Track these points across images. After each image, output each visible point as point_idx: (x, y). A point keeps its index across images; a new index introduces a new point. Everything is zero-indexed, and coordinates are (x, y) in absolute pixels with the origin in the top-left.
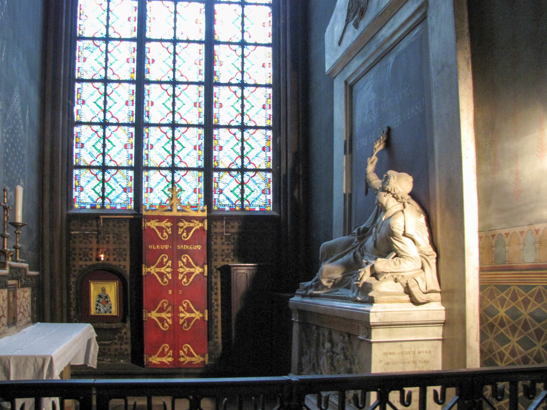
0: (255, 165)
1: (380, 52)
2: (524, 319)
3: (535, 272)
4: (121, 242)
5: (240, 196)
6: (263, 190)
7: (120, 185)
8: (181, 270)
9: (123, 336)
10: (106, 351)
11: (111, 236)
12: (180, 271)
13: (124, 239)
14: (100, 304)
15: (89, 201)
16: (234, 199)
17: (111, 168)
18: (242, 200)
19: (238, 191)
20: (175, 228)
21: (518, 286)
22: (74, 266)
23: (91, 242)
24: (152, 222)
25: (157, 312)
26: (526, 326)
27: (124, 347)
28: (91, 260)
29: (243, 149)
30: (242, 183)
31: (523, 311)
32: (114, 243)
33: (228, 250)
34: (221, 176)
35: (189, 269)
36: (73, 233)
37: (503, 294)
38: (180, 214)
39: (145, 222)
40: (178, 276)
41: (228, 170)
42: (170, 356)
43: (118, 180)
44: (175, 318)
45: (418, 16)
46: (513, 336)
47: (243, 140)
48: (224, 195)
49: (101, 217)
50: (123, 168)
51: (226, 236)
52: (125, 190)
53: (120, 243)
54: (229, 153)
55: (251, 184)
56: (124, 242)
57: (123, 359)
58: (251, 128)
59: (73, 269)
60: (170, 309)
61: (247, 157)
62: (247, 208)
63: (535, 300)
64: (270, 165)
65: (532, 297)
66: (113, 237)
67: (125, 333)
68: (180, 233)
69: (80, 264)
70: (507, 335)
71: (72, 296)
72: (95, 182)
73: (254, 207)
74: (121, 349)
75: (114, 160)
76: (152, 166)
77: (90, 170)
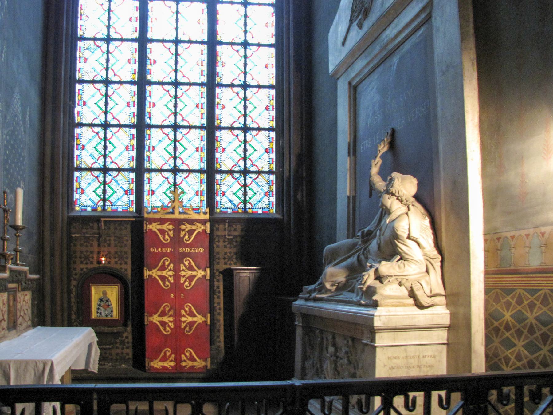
0: (257, 167)
1: (385, 53)
2: (529, 323)
3: (540, 275)
4: (123, 245)
5: (243, 198)
6: (266, 192)
7: (121, 187)
8: (183, 273)
9: (124, 341)
10: (107, 355)
11: (112, 239)
12: (182, 275)
13: (125, 242)
14: (101, 308)
15: (90, 203)
16: (236, 201)
17: (113, 170)
18: (245, 202)
19: (240, 194)
20: (177, 231)
21: (523, 289)
22: (75, 269)
23: (92, 245)
24: (154, 224)
25: (159, 316)
26: (531, 330)
27: (125, 351)
28: (92, 263)
29: (245, 150)
30: (245, 186)
31: (528, 315)
32: (116, 245)
33: (230, 253)
34: (223, 178)
35: (191, 272)
36: (73, 236)
37: (508, 298)
38: (182, 217)
39: (147, 225)
40: (180, 279)
41: (231, 172)
42: (172, 361)
43: (120, 182)
44: (177, 322)
45: (423, 16)
46: (519, 340)
47: (245, 142)
48: (227, 197)
49: (103, 219)
50: (124, 170)
51: (228, 239)
52: (126, 192)
53: (121, 246)
54: (231, 155)
55: (253, 186)
56: (126, 245)
57: (124, 364)
58: (253, 129)
59: (74, 272)
60: (171, 312)
61: (250, 159)
62: (250, 211)
63: (541, 303)
64: (273, 167)
65: (538, 301)
66: (115, 240)
67: (127, 337)
68: (182, 236)
69: (81, 267)
70: (513, 340)
71: (73, 300)
72: (96, 184)
73: (256, 210)
74: (122, 353)
75: (116, 162)
76: (153, 168)
77: (91, 172)
